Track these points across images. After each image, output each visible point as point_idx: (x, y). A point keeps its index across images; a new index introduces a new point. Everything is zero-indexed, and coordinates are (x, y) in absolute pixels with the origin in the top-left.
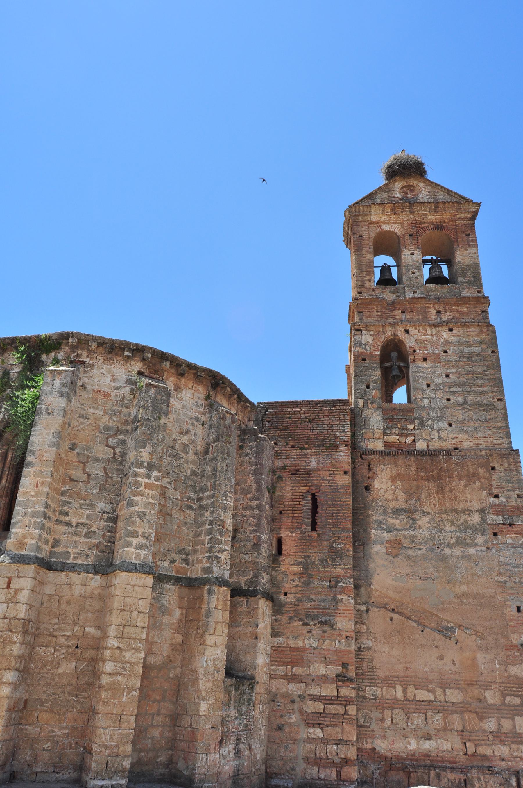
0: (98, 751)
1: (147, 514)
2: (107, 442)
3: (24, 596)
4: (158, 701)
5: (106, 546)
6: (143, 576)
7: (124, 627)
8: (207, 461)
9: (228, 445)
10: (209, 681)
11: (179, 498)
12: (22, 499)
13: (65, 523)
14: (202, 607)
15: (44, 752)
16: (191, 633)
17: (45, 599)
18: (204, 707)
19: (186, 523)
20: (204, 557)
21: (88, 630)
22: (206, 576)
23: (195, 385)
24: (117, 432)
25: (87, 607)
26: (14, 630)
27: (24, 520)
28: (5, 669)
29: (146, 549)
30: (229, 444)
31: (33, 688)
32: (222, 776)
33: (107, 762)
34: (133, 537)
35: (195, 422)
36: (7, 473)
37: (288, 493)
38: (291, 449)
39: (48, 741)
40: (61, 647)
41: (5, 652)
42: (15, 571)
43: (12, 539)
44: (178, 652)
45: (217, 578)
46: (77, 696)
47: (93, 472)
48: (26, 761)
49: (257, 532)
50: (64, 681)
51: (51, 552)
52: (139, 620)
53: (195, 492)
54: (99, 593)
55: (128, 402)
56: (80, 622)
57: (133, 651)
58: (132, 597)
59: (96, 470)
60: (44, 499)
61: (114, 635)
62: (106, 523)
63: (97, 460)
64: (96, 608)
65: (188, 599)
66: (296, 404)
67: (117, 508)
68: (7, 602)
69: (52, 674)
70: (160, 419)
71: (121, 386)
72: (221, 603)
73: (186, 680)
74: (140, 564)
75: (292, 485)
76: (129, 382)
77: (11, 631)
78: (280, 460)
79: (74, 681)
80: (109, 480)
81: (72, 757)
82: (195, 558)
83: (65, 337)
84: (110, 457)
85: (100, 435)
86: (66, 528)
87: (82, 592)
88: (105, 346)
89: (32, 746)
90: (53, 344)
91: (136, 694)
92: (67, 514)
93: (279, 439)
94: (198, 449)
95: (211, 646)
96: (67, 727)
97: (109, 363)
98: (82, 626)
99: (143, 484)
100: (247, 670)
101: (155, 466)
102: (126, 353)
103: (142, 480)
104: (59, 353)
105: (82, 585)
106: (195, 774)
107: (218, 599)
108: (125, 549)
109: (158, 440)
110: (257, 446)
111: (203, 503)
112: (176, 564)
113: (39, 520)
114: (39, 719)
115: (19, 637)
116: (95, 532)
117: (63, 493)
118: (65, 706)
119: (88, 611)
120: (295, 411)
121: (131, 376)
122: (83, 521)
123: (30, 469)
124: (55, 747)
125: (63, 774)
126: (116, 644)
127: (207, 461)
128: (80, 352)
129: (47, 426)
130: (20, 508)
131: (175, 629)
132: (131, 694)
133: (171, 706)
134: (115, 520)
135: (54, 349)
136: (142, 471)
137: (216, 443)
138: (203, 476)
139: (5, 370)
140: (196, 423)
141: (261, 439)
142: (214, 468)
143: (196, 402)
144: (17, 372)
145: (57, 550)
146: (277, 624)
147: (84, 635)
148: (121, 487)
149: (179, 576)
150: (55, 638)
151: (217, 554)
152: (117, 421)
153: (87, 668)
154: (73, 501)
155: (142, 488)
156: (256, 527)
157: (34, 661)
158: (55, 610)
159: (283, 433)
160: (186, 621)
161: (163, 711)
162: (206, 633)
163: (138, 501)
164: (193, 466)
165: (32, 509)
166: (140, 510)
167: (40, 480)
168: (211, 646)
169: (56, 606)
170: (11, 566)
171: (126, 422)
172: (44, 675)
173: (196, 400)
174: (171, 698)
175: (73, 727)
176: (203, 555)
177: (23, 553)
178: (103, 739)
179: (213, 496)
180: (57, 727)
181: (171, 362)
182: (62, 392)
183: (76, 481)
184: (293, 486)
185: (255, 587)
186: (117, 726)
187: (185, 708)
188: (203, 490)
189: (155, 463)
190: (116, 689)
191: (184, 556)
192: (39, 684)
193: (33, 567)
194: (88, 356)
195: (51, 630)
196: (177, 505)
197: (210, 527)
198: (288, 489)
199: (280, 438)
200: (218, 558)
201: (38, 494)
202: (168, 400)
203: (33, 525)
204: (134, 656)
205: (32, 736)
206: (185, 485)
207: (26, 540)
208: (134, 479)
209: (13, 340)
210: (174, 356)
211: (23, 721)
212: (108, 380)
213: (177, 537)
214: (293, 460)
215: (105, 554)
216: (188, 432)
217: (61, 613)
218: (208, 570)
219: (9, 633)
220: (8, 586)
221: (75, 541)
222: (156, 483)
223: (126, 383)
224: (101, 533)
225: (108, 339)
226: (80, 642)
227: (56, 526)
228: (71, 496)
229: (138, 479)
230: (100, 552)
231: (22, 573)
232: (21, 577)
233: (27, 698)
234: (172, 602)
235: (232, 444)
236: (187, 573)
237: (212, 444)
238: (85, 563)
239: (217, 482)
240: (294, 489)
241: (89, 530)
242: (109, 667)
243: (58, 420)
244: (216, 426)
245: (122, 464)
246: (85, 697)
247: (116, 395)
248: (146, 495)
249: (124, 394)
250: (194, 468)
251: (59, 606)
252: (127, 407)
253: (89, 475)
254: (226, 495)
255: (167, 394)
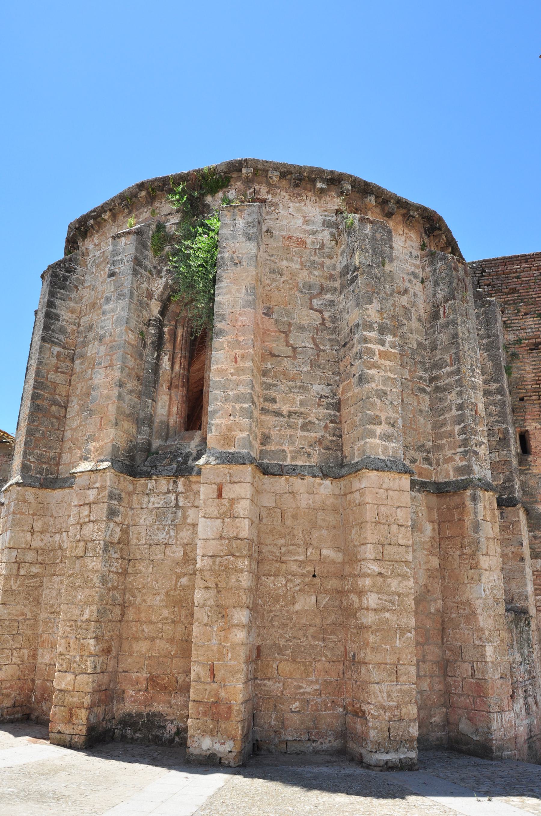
0: (376, 714)
1: (388, 393)
2: (311, 304)
3: (243, 508)
4: (421, 644)
5: (331, 441)
6: (397, 476)
7: (383, 545)
8: (438, 329)
9: (465, 304)
10: (490, 617)
11: (409, 377)
12: (218, 379)
13: (274, 412)
14: (465, 518)
15: (292, 714)
16: (452, 553)
17: (264, 513)
18: (489, 650)
19: (421, 411)
20: (455, 454)
21: (325, 552)
22: (463, 478)
23: (406, 231)
24: (322, 290)
25: (320, 522)
26: (237, 554)
27: (226, 407)
28: (234, 607)
29: (394, 441)
30: (467, 303)
31: (265, 631)
32: (519, 740)
33: (389, 730)
34: (375, 424)
35: (412, 279)
36: (179, 355)
37: (529, 373)
38: (524, 317)
39: (295, 700)
40: (293, 576)
41: (231, 584)
42: (225, 475)
43: (213, 433)
44: (436, 580)
45: (479, 480)
46: (324, 640)
47: (299, 344)
48: (271, 727)
49: (503, 423)
50: (304, 621)
51: (261, 451)
52: (400, 536)
53: (425, 370)
54: (332, 504)
55: (329, 250)
56: (313, 542)
57: (400, 578)
58: (388, 505)
59: (302, 340)
60: (249, 377)
61: (372, 556)
62: (326, 411)
63: (302, 328)
64: (331, 524)
65: (438, 509)
66: (526, 258)
67: (337, 390)
68: (222, 517)
69: (288, 611)
70: (384, 265)
71: (317, 230)
72: (489, 512)
73: (454, 615)
74: (390, 460)
75: (534, 363)
76: (326, 224)
77: (233, 555)
78: (511, 332)
79: (318, 621)
80: (322, 354)
81: (329, 720)
82: (441, 457)
83: (236, 167)
84: (318, 323)
85: (301, 295)
86: (277, 418)
87: (311, 502)
88: (289, 177)
89: (276, 706)
90: (220, 180)
91: (412, 636)
92: (274, 400)
93: (506, 306)
94: (421, 314)
95: (486, 570)
96: (317, 682)
97: (296, 200)
98: (317, 548)
99: (377, 353)
100: (514, 601)
101: (387, 328)
102: (319, 185)
103: (374, 347)
104: (228, 192)
105: (308, 493)
106: (492, 740)
107: (485, 507)
108: (367, 440)
109: (385, 293)
110: (485, 313)
111: (439, 384)
112: (417, 464)
113: (246, 405)
114: (280, 672)
115: (246, 563)
116: (314, 423)
117: (265, 373)
118: (310, 654)
119: (321, 527)
120: (524, 268)
121: (328, 216)
122: (297, 409)
123: (222, 339)
124: (306, 708)
125: (322, 743)
126: (377, 570)
127: (438, 329)
128: (257, 187)
129: (235, 281)
130: (218, 392)
131: (429, 550)
132: (406, 636)
133: (437, 651)
134: (337, 406)
135: (221, 187)
136: (372, 334)
137: (449, 303)
138: (435, 348)
139: (159, 222)
140: (414, 280)
141: (491, 304)
142: (452, 335)
143: (411, 253)
144: (175, 224)
145: (267, 448)
146: (537, 542)
147: (321, 560)
148: (338, 362)
149: (423, 480)
150: (284, 565)
151: (474, 448)
152: (319, 276)
153: (331, 603)
154: (279, 383)
155: (376, 358)
156: (499, 417)
157: (261, 596)
158: (279, 528)
159: (510, 297)
160: (441, 539)
161: (429, 657)
162: (477, 552)
163: (373, 375)
164: (418, 336)
165: (234, 392)
166: (378, 388)
167: (238, 352)
168: (486, 570)
169: (280, 521)
170: (218, 468)
171: (331, 277)
172: (277, 614)
173: (410, 250)
174: (435, 639)
175: (325, 681)
176: (453, 451)
177: (232, 450)
178: (380, 698)
179: (458, 372)
180: (304, 681)
181: (377, 197)
182: (249, 234)
183: (279, 356)
184: (535, 365)
185: (510, 494)
186: (395, 680)
187: (458, 652)
188: (437, 366)
189: (387, 324)
190: (385, 630)
191: (425, 454)
192: (273, 625)
193: (250, 469)
194: (268, 193)
195: (278, 554)
196: (408, 387)
197: (460, 412)
198: (529, 368)
199: (507, 304)
200: (476, 453)
201: (239, 371)
202: (390, 240)
203: (239, 413)
204: (401, 585)
205: (274, 694)
206: (413, 361)
207: (233, 433)
208: (364, 345)
209: (165, 181)
210: (380, 188)
211: (259, 674)
212: (300, 222)
213: (413, 429)
214: (529, 330)
215: (331, 451)
216: (406, 291)
217: (288, 531)
218: (467, 470)
219: (231, 558)
220: (220, 496)
221: (291, 436)
222: (393, 351)
223: (323, 226)
224: (322, 424)
225: (294, 166)
226: (317, 568)
227: (262, 417)
228: (275, 377)
229: (369, 346)
230: (325, 449)
231: (236, 477)
232: (235, 483)
233: (260, 643)
234: (420, 515)
235: (470, 304)
236: (431, 477)
237: (443, 305)
238: (308, 464)
239: (461, 353)
240: (537, 369)
241: (306, 421)
242: (372, 600)
243: (248, 274)
244: (447, 279)
245: (335, 332)
246: (334, 642)
247: (313, 242)
248: (383, 367)
249: (322, 240)
250: (421, 339)
251: (283, 523)
252: (330, 257)
253: (294, 349)
254: (473, 371)
255: (388, 232)
